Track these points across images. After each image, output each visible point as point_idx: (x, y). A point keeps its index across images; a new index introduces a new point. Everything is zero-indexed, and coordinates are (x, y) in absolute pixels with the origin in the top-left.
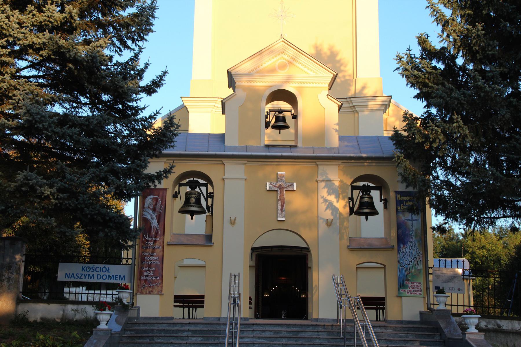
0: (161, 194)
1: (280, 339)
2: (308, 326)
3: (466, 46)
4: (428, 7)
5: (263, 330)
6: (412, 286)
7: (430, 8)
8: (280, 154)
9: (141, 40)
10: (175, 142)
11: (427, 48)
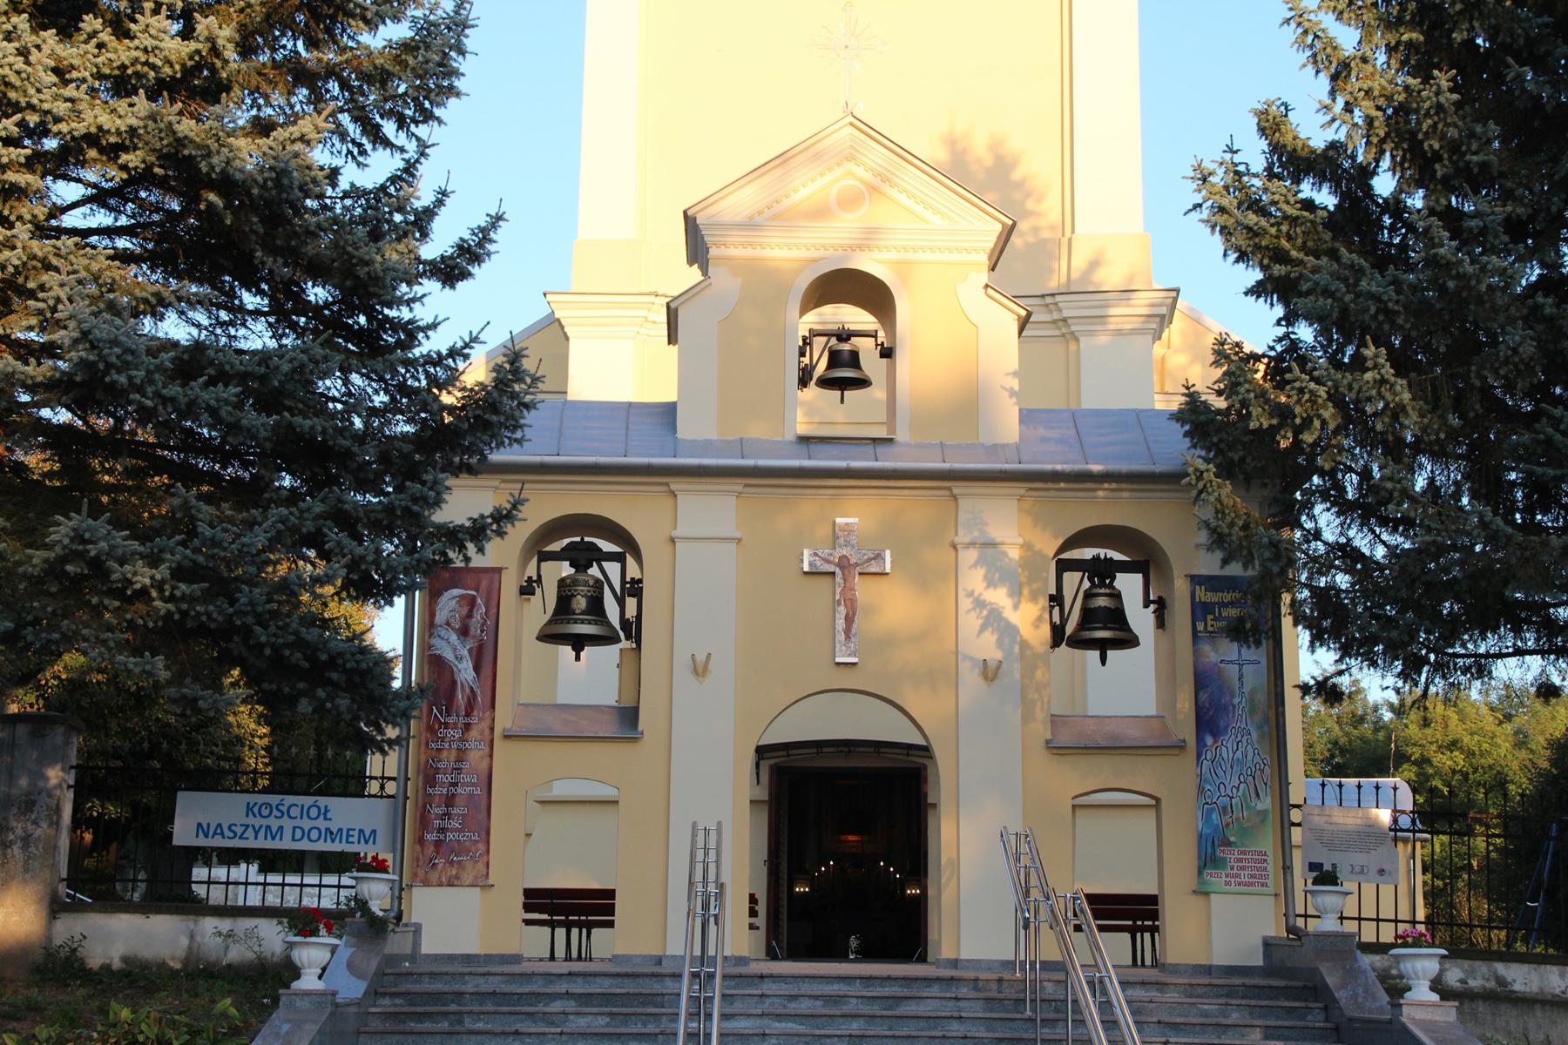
0: (484, 583)
2: (928, 981)
3: (1402, 140)
4: (1287, 21)
6: (1239, 860)
7: (1293, 25)
9: (425, 121)
10: (526, 429)
11: (1284, 146)
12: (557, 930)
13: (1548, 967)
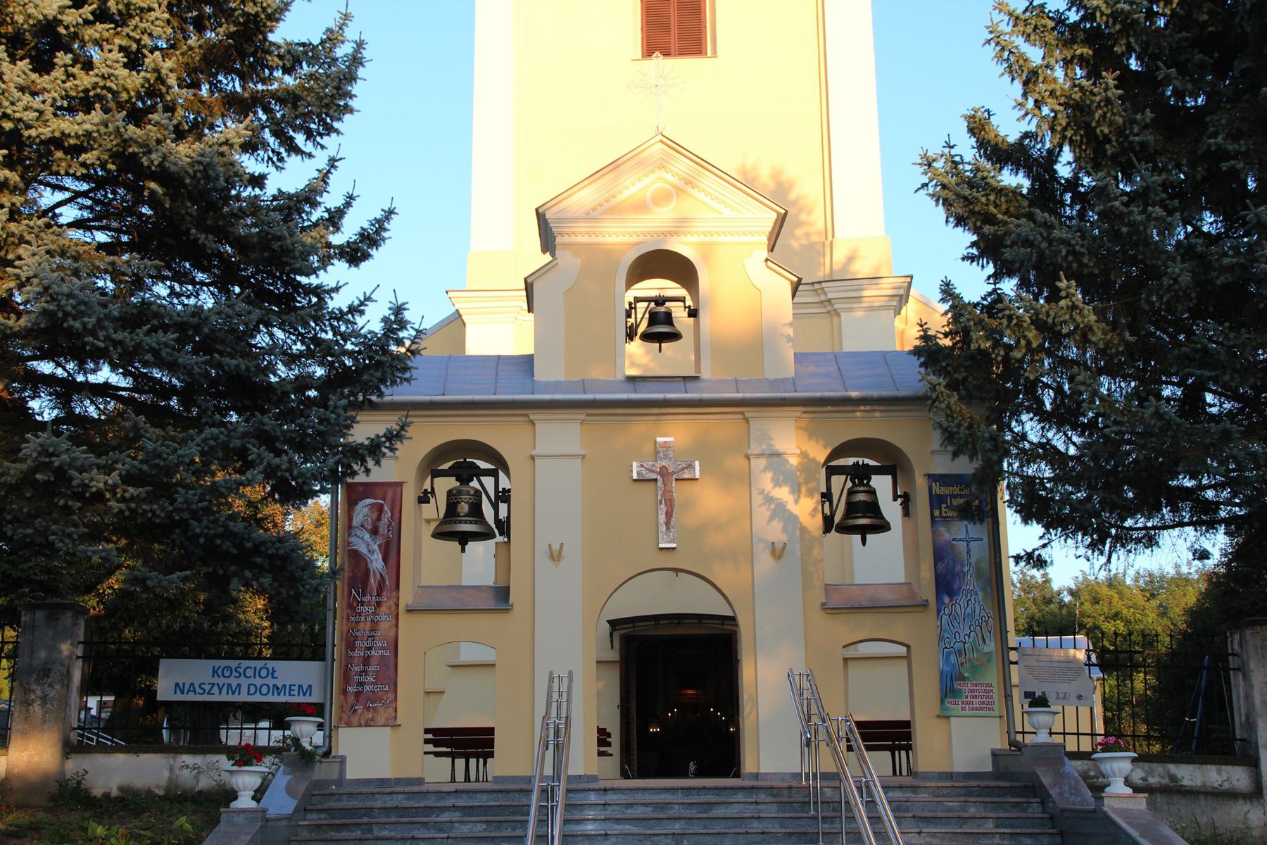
0: (389, 495)
1: (667, 822)
3: (1079, 128)
4: (988, 42)
5: (629, 802)
6: (972, 691)
7: (993, 44)
8: (660, 396)
10: (413, 371)
11: (989, 142)
12: (456, 760)
13: (1209, 766)
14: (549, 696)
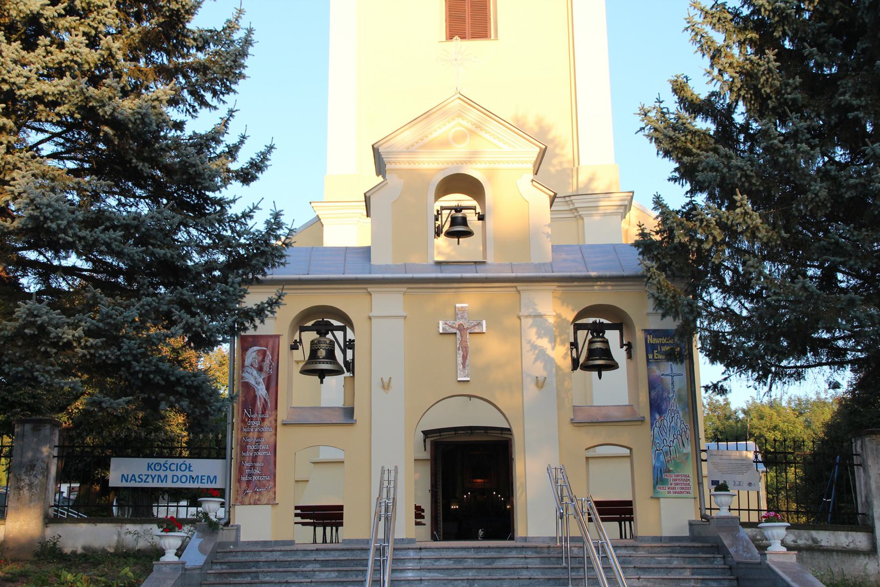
0: (270, 344)
1: (463, 571)
3: (750, 89)
4: (687, 29)
6: (675, 480)
7: (690, 31)
8: (458, 275)
10: (287, 257)
12: (317, 528)
13: (839, 532)
14: (381, 484)
